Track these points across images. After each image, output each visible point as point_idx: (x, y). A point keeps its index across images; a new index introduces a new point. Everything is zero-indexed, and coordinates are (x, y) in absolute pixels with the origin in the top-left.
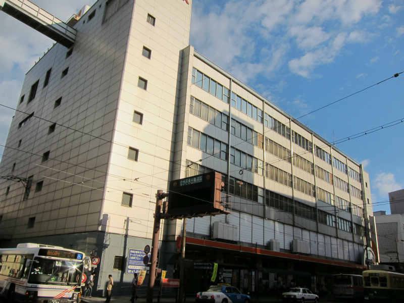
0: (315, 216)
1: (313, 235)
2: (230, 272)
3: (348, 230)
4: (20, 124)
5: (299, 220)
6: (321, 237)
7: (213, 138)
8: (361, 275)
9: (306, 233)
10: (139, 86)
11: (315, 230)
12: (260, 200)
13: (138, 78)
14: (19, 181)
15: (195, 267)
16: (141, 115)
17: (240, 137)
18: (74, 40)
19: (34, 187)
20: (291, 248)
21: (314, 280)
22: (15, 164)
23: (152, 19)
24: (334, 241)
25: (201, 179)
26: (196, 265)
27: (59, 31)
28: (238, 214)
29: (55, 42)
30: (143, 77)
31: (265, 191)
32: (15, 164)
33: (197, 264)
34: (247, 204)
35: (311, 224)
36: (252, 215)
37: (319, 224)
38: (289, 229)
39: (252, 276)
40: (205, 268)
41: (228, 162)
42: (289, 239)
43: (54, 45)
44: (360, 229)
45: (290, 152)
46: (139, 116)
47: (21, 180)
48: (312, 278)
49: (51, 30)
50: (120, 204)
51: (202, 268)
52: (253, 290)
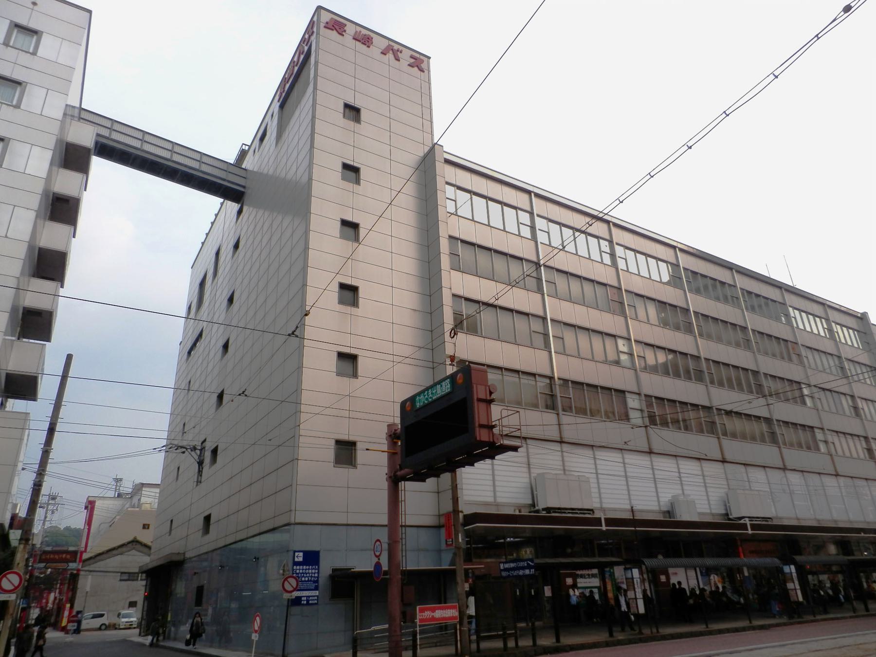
0: (773, 434)
1: (776, 475)
2: (593, 576)
3: (862, 456)
4: (189, 353)
5: (734, 448)
6: (795, 478)
7: (601, 333)
8: (465, 568)
9: (758, 475)
10: (343, 236)
11: (719, 457)
12: (635, 416)
13: (339, 224)
14: (184, 452)
15: (504, 574)
16: (354, 289)
17: (646, 321)
18: (244, 187)
19: (208, 455)
20: (726, 510)
21: (791, 573)
22: (184, 425)
23: (353, 111)
24: (830, 481)
25: (449, 386)
26: (506, 570)
27: (186, 166)
28: (620, 455)
29: (222, 200)
30: (349, 218)
31: (643, 397)
32: (184, 425)
33: (507, 566)
34: (613, 431)
35: (767, 453)
36: (699, 459)
37: (785, 451)
38: (713, 469)
39: (633, 578)
40: (521, 573)
41: (550, 352)
42: (717, 493)
43: (222, 204)
44: (814, 432)
45: (686, 311)
46: (561, 340)
47: (187, 449)
48: (786, 569)
49: (227, 188)
50: (332, 464)
51: (515, 573)
52: (642, 610)
